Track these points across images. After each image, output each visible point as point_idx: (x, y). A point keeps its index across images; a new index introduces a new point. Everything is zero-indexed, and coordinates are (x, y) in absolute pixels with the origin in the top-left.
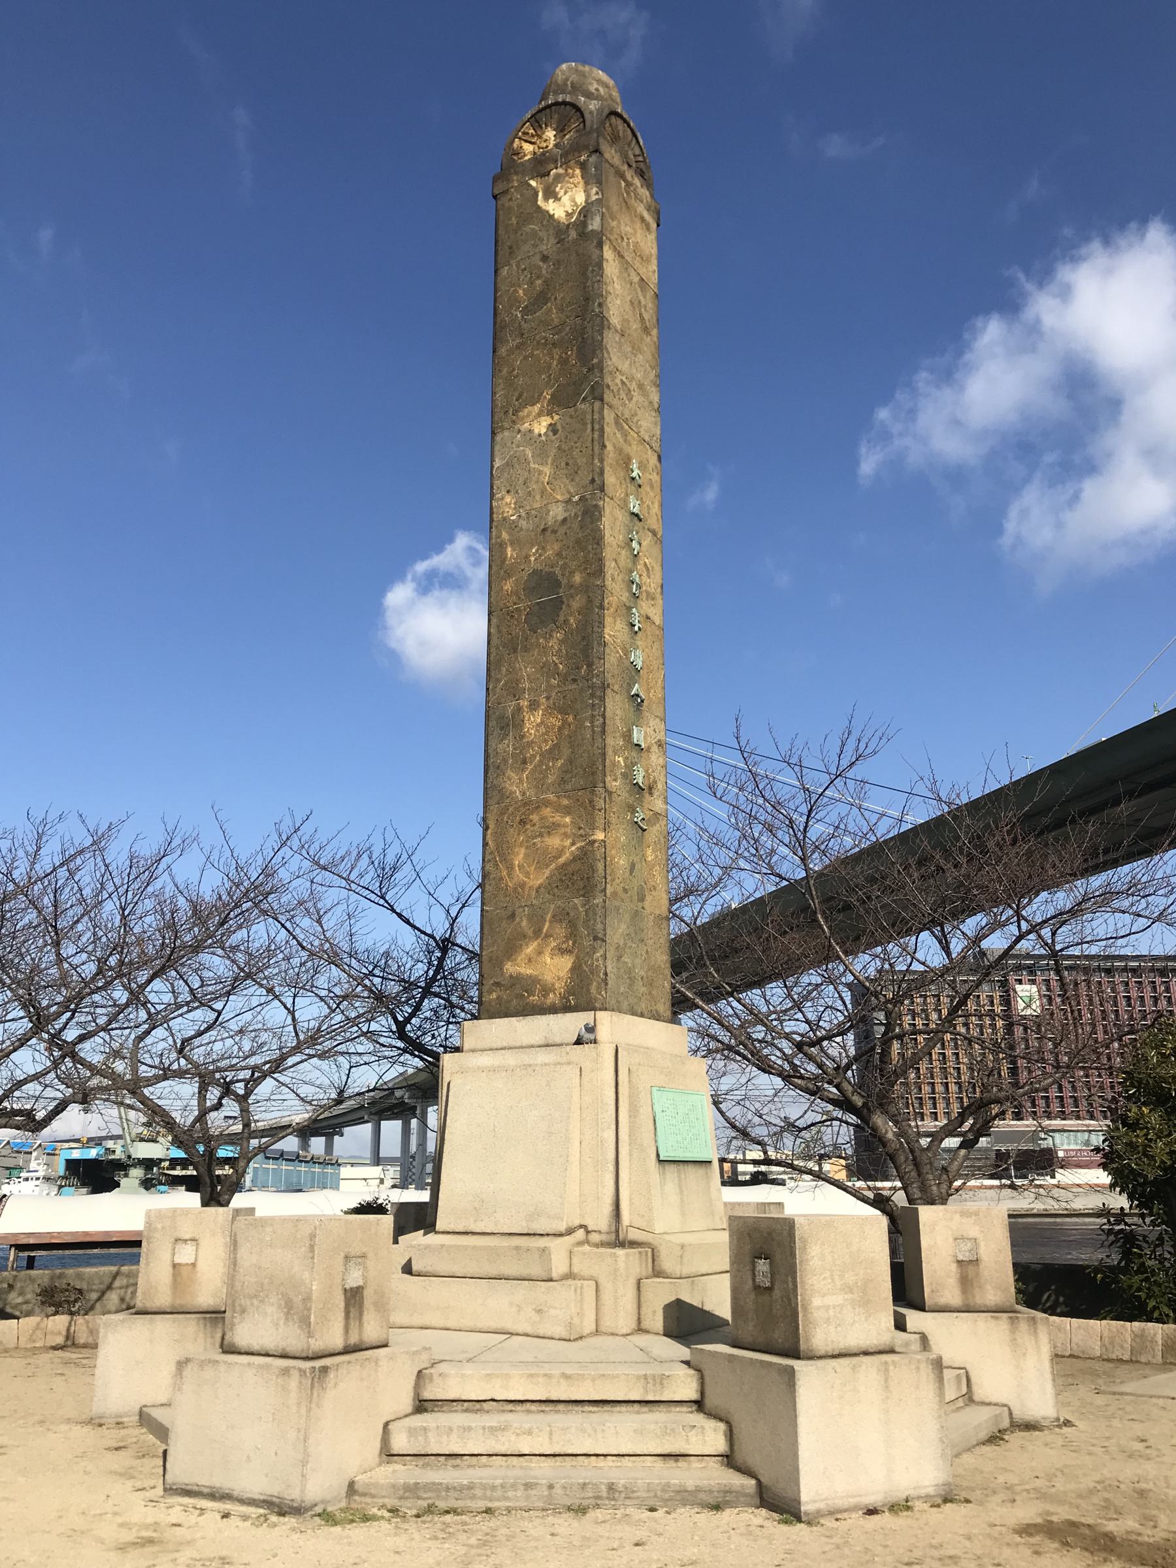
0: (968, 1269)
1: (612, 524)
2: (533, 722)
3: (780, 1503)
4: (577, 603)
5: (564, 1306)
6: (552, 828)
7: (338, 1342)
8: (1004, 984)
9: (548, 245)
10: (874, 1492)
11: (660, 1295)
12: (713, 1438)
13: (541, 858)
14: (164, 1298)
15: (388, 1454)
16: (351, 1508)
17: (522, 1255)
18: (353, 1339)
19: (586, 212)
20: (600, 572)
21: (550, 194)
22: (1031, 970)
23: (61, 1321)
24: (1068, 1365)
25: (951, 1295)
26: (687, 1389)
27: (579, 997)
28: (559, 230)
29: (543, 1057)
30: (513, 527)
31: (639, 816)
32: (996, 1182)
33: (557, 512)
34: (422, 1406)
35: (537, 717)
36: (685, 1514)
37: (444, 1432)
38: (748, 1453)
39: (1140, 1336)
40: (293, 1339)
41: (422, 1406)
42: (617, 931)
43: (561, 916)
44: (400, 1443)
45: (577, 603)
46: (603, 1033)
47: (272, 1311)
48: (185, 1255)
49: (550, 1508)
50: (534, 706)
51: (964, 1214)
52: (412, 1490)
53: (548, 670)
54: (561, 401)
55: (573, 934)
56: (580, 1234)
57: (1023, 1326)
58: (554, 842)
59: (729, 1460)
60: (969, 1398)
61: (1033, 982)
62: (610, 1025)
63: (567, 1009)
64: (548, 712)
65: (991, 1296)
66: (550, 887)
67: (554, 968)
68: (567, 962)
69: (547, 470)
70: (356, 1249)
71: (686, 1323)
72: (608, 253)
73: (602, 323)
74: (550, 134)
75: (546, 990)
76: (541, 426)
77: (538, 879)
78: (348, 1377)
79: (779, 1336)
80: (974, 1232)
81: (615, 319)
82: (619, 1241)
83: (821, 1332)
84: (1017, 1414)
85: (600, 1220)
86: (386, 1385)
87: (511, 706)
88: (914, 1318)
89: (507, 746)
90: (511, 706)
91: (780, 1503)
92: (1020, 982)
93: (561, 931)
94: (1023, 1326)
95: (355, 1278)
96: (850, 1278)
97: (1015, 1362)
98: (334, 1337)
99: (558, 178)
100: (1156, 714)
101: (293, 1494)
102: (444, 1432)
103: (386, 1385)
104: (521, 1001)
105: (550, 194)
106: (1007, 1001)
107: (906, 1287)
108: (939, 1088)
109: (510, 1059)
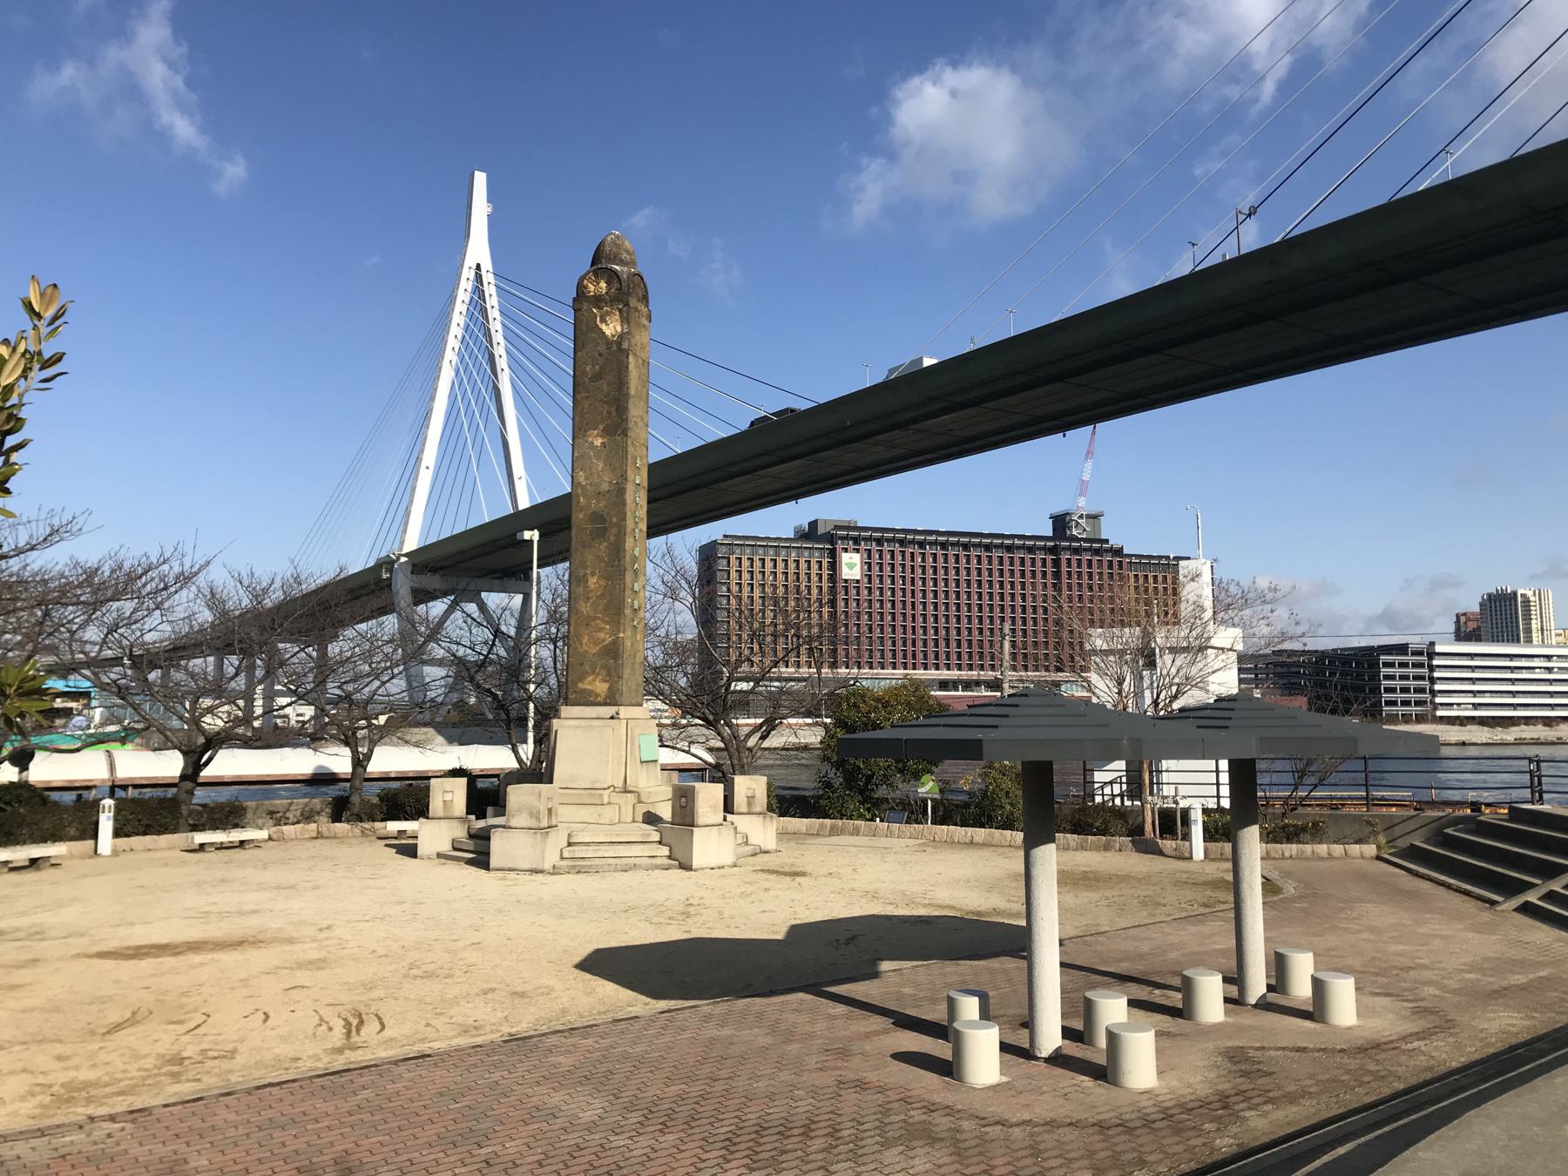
0: (751, 799)
1: (630, 488)
2: (592, 581)
3: (686, 866)
4: (614, 531)
5: (609, 813)
6: (600, 630)
8: (833, 553)
9: (602, 348)
11: (642, 809)
12: (665, 851)
13: (596, 642)
14: (440, 813)
16: (555, 871)
17: (591, 795)
19: (621, 336)
20: (624, 519)
21: (603, 320)
22: (856, 540)
23: (313, 826)
24: (783, 835)
25: (744, 809)
26: (657, 838)
27: (611, 700)
28: (608, 342)
29: (597, 723)
30: (583, 488)
32: (809, 721)
33: (605, 487)
34: (570, 844)
35: (594, 579)
36: (657, 872)
37: (579, 852)
38: (677, 854)
39: (821, 825)
40: (533, 823)
41: (570, 844)
42: (626, 673)
43: (604, 667)
44: (566, 855)
45: (614, 531)
46: (622, 715)
47: (525, 815)
48: (448, 797)
50: (593, 574)
53: (601, 560)
54: (607, 432)
55: (609, 674)
58: (602, 635)
59: (670, 857)
60: (746, 843)
61: (857, 551)
62: (625, 712)
63: (606, 704)
64: (600, 578)
65: (758, 809)
66: (599, 653)
67: (601, 687)
68: (605, 686)
69: (601, 465)
71: (651, 819)
72: (631, 359)
73: (626, 396)
74: (603, 285)
75: (597, 695)
76: (598, 442)
77: (594, 650)
79: (688, 821)
81: (632, 392)
82: (626, 791)
83: (700, 820)
85: (619, 783)
86: (558, 840)
87: (582, 572)
88: (729, 817)
89: (581, 590)
90: (582, 572)
91: (686, 866)
92: (846, 550)
93: (604, 672)
97: (764, 831)
98: (545, 823)
99: (608, 313)
100: (972, 347)
101: (540, 867)
102: (579, 852)
103: (558, 840)
104: (587, 700)
105: (603, 320)
106: (834, 566)
107: (728, 807)
109: (583, 723)
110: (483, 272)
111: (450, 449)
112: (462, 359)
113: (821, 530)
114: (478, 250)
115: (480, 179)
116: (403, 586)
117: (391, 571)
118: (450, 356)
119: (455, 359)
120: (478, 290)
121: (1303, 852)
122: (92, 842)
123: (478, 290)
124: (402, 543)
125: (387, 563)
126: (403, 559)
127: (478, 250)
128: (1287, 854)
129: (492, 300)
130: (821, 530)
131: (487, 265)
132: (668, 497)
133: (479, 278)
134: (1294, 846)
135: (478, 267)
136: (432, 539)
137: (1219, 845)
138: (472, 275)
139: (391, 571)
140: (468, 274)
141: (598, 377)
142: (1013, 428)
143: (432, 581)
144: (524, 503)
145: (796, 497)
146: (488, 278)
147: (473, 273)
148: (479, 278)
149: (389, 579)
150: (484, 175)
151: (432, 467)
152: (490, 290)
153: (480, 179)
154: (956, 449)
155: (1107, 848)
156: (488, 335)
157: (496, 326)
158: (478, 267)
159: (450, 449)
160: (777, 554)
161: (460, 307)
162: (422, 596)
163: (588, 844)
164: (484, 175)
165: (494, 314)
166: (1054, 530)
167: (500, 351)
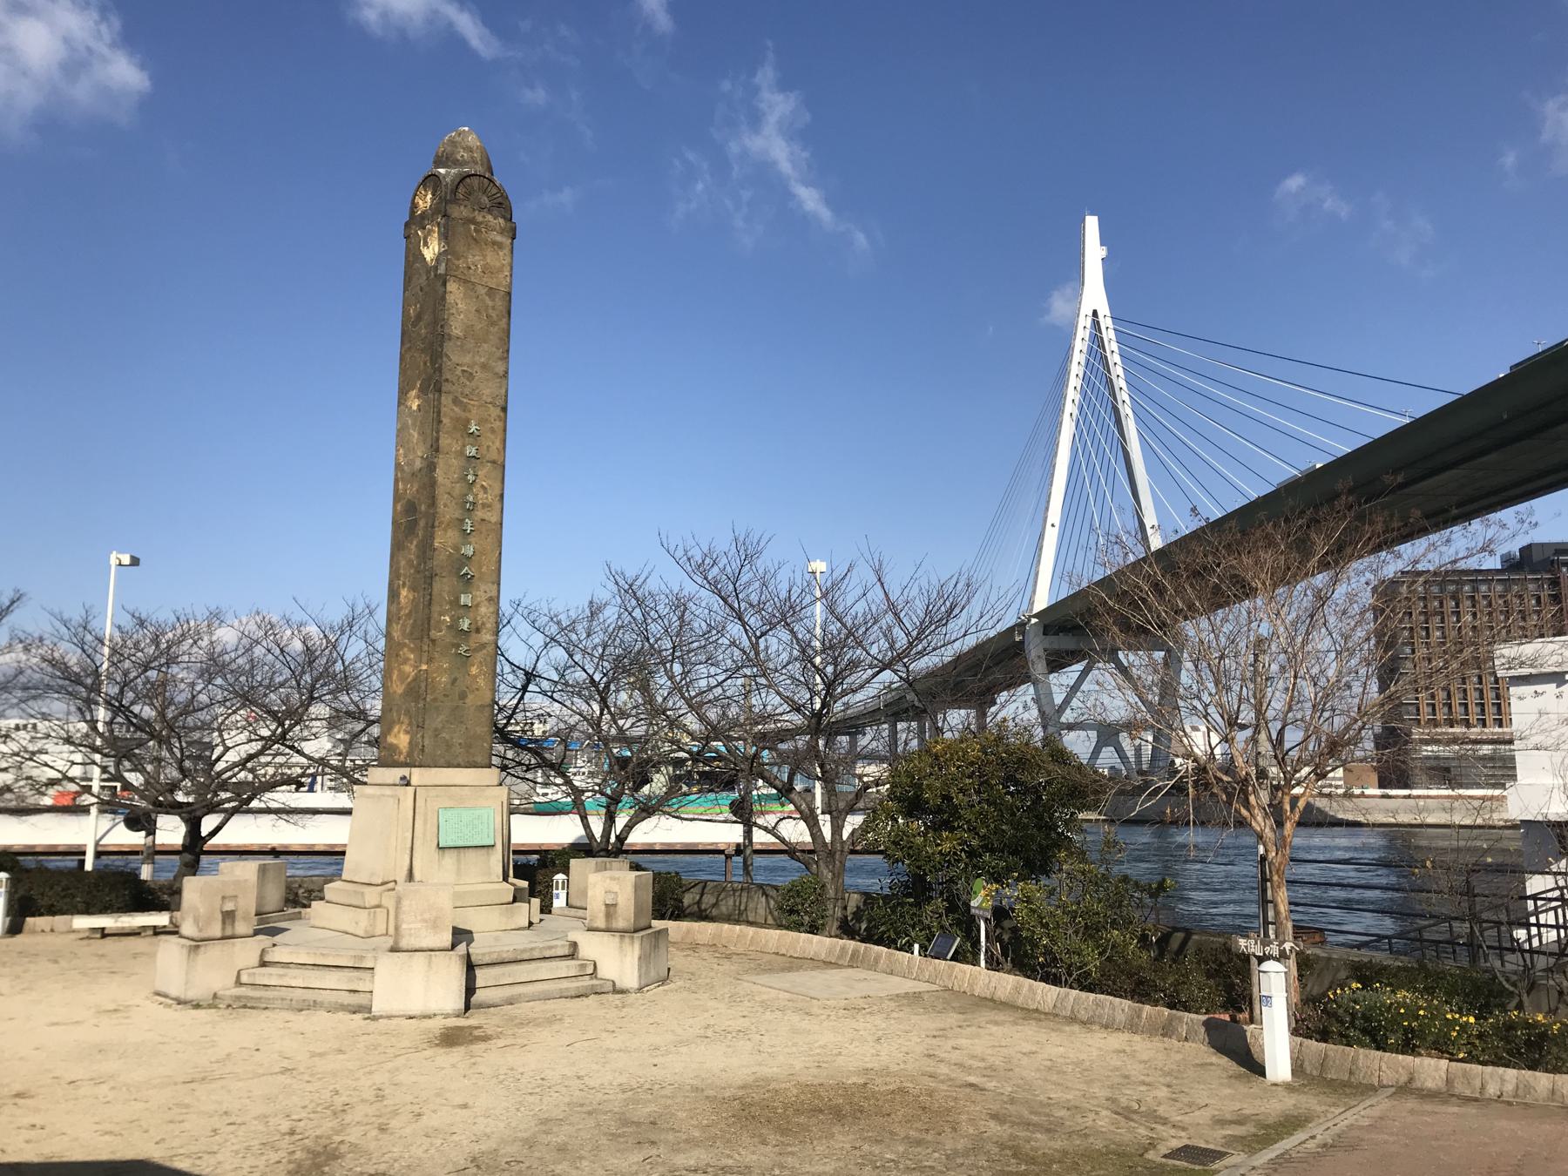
0: (610, 909)
7: (218, 934)
10: (416, 1009)
15: (239, 983)
18: (229, 932)
31: (462, 650)
34: (263, 964)
39: (843, 948)
49: (290, 1009)
51: (612, 879)
52: (238, 998)
56: (391, 885)
57: (627, 940)
60: (594, 974)
65: (621, 923)
70: (230, 893)
78: (213, 952)
80: (616, 889)
84: (618, 985)
94: (627, 940)
95: (229, 906)
96: (427, 916)
108: (1473, 696)
113: (1537, 557)
114: (1094, 295)
115: (1092, 224)
116: (1036, 650)
117: (1023, 633)
118: (1070, 408)
119: (1078, 397)
120: (1097, 339)
121: (1529, 1088)
123: (1097, 339)
124: (1031, 603)
125: (1021, 626)
126: (1034, 621)
128: (1492, 1090)
129: (1112, 346)
130: (1537, 557)
133: (1096, 324)
134: (1511, 1074)
135: (1095, 313)
137: (1350, 1051)
138: (1089, 323)
139: (1023, 633)
140: (1084, 322)
141: (419, 317)
143: (1065, 642)
146: (1106, 322)
147: (1089, 320)
148: (1096, 324)
149: (1022, 642)
150: (1095, 219)
151: (1057, 525)
152: (1109, 335)
153: (1092, 224)
155: (1167, 1031)
156: (1110, 384)
157: (1118, 371)
158: (1095, 313)
160: (1507, 590)
162: (1057, 663)
163: (287, 965)
164: (1095, 219)
167: (1126, 410)
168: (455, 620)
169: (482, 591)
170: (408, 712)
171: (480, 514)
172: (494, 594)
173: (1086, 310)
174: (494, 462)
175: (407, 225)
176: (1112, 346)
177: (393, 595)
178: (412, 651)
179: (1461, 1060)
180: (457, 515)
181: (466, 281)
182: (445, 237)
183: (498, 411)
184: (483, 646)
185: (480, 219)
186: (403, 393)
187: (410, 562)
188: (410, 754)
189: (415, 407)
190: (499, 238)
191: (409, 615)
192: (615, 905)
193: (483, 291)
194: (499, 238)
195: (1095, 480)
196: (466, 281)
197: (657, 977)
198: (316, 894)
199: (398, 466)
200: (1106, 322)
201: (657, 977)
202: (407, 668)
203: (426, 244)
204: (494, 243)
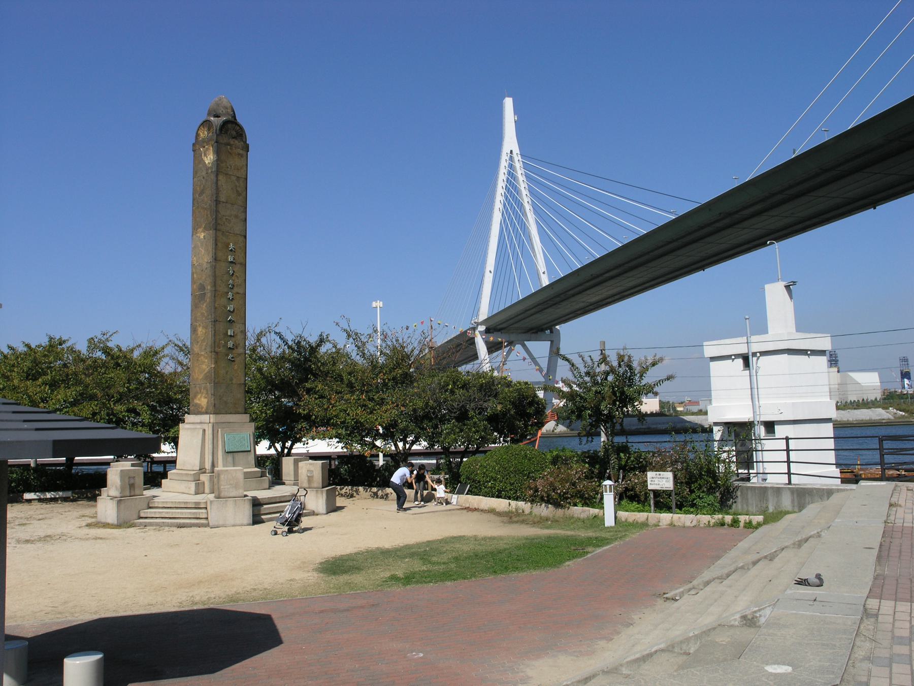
0: (310, 479)
80: (312, 469)
95: (132, 481)
110: (514, 155)
111: (502, 259)
112: (506, 198)
114: (510, 142)
115: (508, 103)
119: (501, 207)
120: (511, 174)
122: (325, 512)
123: (511, 174)
127: (510, 142)
129: (523, 185)
131: (516, 150)
132: (766, 210)
133: (511, 158)
135: (511, 152)
136: (495, 312)
142: (838, 207)
144: (545, 281)
145: (874, 204)
148: (511, 158)
152: (518, 165)
153: (508, 103)
154: (663, 279)
158: (511, 152)
159: (502, 259)
161: (499, 199)
165: (521, 178)
166: (764, 289)
168: (226, 343)
169: (238, 328)
170: (205, 388)
171: (236, 290)
172: (242, 329)
173: (506, 149)
174: (241, 264)
175: (194, 145)
176: (523, 185)
177: (194, 330)
178: (206, 358)
179: (662, 501)
180: (226, 290)
181: (226, 174)
182: (218, 152)
183: (243, 238)
184: (239, 355)
185: (232, 143)
186: (195, 230)
187: (202, 314)
188: (207, 408)
189: (202, 237)
190: (241, 152)
191: (203, 341)
192: (312, 477)
193: (234, 178)
194: (241, 152)
195: (519, 263)
196: (226, 174)
197: (332, 508)
198: (164, 475)
199: (193, 265)
200: (517, 158)
201: (332, 508)
202: (204, 366)
203: (205, 155)
204: (239, 154)
